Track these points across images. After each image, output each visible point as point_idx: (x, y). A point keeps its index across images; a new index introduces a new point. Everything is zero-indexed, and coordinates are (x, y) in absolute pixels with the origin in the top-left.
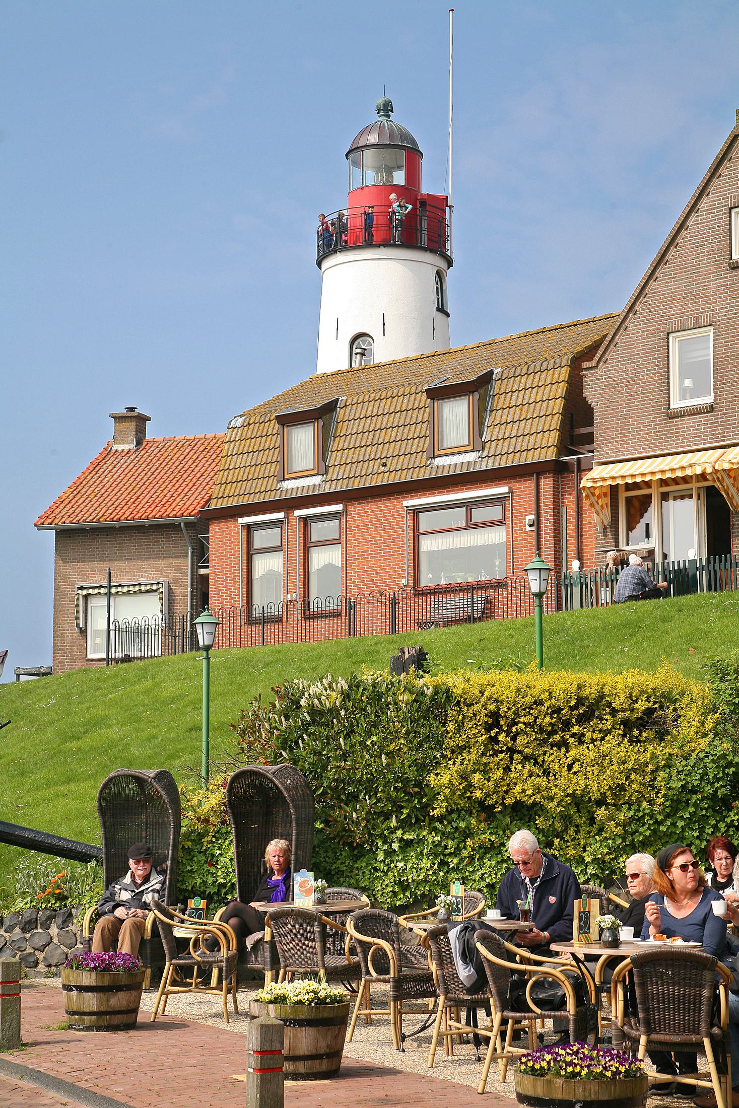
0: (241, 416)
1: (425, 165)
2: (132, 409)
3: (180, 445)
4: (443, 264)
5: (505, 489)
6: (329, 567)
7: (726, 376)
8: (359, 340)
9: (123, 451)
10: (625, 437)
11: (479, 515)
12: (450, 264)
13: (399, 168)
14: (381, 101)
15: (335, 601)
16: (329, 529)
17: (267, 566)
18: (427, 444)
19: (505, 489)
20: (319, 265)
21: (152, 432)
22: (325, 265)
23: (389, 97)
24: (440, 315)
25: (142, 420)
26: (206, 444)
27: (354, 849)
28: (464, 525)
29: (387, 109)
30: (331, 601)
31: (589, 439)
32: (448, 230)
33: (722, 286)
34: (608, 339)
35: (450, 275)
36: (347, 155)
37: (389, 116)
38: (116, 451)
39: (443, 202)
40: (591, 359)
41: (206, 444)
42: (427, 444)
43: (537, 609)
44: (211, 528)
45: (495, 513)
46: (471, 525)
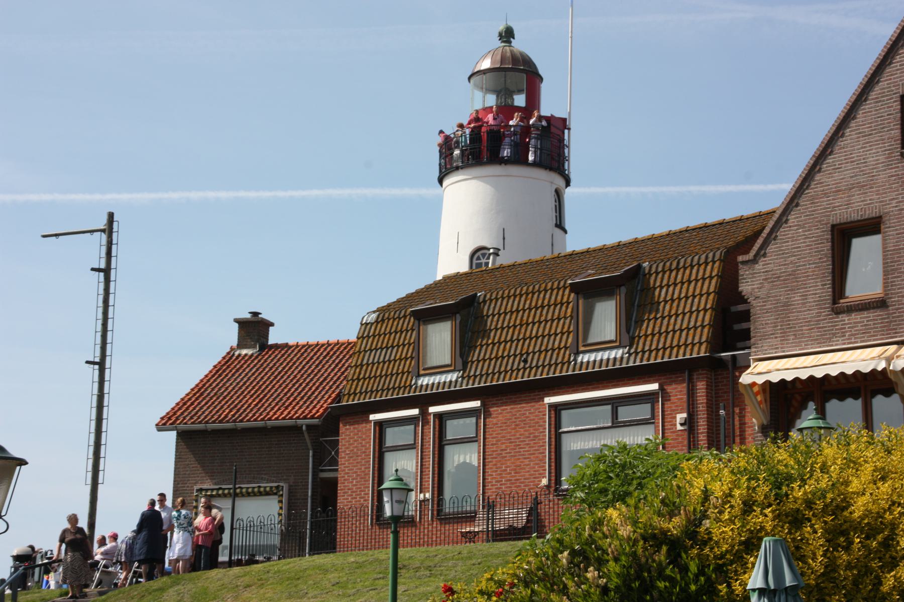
0: (374, 312)
1: (545, 89)
2: (255, 314)
3: (303, 351)
4: (561, 182)
5: (655, 386)
6: (465, 465)
7: (897, 269)
8: (479, 253)
9: (246, 355)
10: (785, 333)
11: (625, 413)
12: (568, 183)
13: (520, 91)
14: (501, 27)
15: (473, 500)
16: (466, 427)
17: (403, 464)
18: (570, 340)
19: (655, 386)
20: (441, 181)
21: (274, 337)
22: (446, 182)
23: (511, 24)
24: (558, 231)
25: (266, 325)
26: (329, 349)
27: (117, 561)
28: (610, 424)
29: (507, 35)
30: (469, 500)
31: (746, 335)
32: (566, 151)
33: (892, 176)
34: (767, 231)
35: (569, 193)
36: (469, 78)
37: (510, 42)
38: (239, 355)
39: (563, 124)
40: (747, 252)
41: (329, 349)
42: (570, 340)
43: (391, 536)
44: (343, 429)
45: (643, 411)
46: (616, 424)
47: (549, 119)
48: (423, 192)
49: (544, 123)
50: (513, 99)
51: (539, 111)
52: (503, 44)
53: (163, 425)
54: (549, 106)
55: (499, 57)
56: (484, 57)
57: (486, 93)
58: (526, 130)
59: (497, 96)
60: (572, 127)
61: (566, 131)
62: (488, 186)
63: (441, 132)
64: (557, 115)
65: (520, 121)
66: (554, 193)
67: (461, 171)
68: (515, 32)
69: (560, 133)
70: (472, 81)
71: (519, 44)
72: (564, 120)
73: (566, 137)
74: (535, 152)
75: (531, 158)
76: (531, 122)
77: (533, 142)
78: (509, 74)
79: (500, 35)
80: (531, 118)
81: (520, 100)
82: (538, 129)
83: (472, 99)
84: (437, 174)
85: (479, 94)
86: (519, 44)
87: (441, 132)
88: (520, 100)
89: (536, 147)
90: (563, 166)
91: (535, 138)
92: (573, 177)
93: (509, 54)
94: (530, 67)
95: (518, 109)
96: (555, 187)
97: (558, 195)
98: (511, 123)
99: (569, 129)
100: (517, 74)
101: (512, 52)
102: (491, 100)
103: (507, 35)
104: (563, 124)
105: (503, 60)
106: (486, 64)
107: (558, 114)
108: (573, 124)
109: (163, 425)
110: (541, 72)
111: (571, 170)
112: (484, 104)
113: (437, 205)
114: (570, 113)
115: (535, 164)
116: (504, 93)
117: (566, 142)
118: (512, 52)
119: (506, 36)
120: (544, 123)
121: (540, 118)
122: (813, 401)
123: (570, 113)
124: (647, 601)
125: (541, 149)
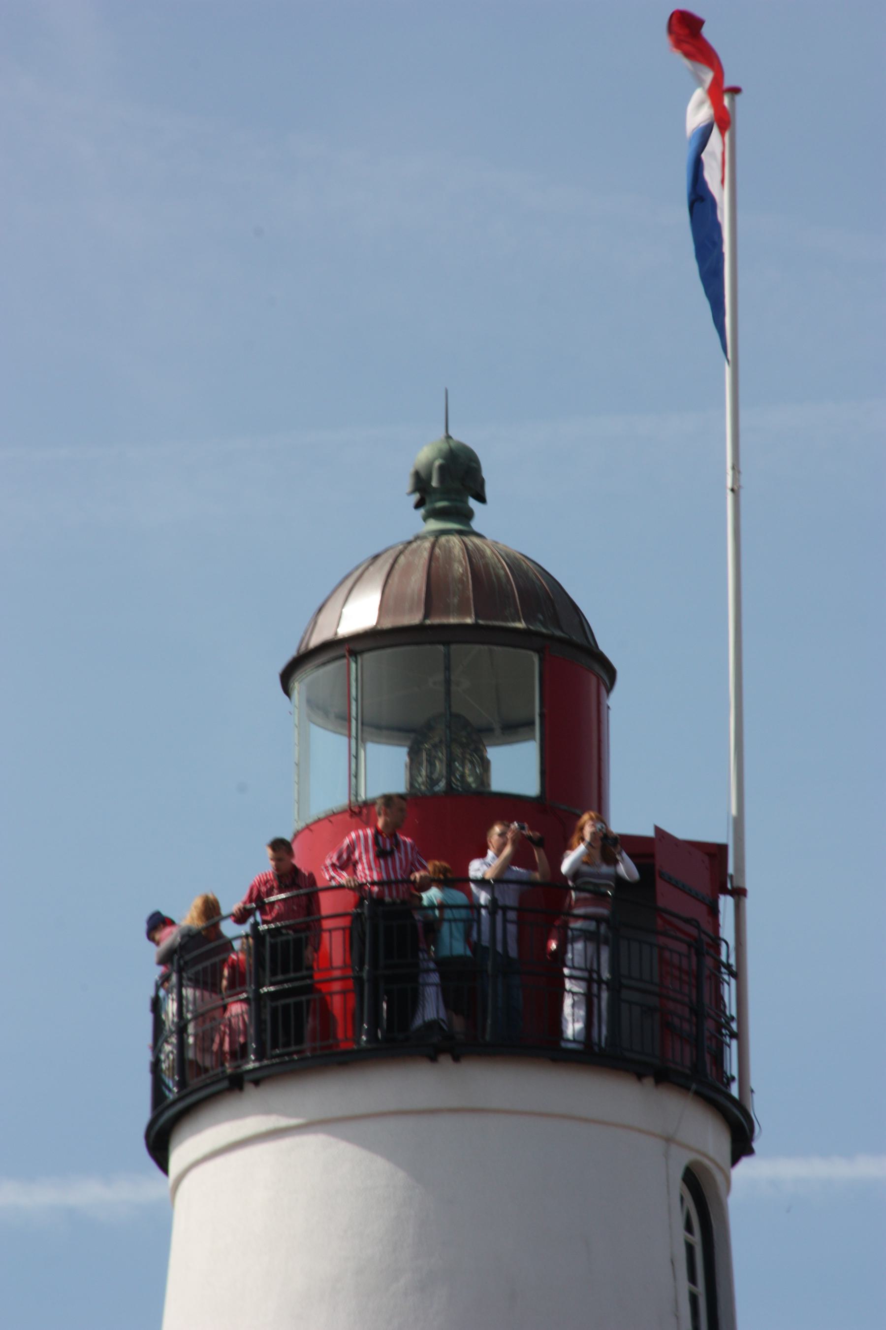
1: (630, 723)
4: (708, 1137)
12: (742, 1143)
13: (512, 730)
14: (425, 452)
20: (159, 1146)
22: (182, 1153)
23: (465, 435)
29: (452, 485)
32: (729, 992)
35: (748, 1185)
36: (286, 677)
37: (467, 516)
39: (711, 869)
47: (650, 850)
48: (89, 1194)
49: (626, 868)
50: (485, 764)
51: (601, 815)
52: (434, 525)
53: (657, 830)
54: (651, 787)
55: (417, 582)
56: (350, 582)
57: (361, 740)
58: (541, 902)
59: (414, 754)
60: (750, 883)
61: (726, 904)
62: (380, 1164)
63: (158, 923)
64: (683, 831)
65: (515, 859)
66: (677, 1185)
67: (252, 1095)
68: (487, 473)
69: (699, 912)
70: (298, 687)
71: (503, 524)
72: (714, 855)
73: (727, 931)
74: (589, 1001)
75: (573, 1025)
76: (565, 867)
77: (577, 951)
78: (468, 654)
79: (420, 483)
80: (566, 846)
81: (515, 768)
82: (598, 896)
83: (302, 767)
84: (142, 1112)
85: (330, 746)
86: (503, 524)
87: (158, 923)
88: (515, 768)
89: (591, 979)
90: (719, 1060)
91: (587, 936)
92: (761, 1109)
93: (460, 568)
94: (556, 621)
95: (510, 806)
96: (680, 1161)
97: (702, 1199)
98: (477, 869)
99: (739, 893)
100: (495, 650)
101: (471, 555)
102: (387, 770)
103: (452, 485)
104: (711, 869)
105: (435, 592)
106: (361, 613)
107: (688, 827)
108: (756, 871)
109: (657, 830)
110: (605, 646)
111: (755, 1081)
112: (353, 789)
113: (147, 1247)
114: (738, 823)
115: (590, 1056)
116: (445, 735)
117: (727, 954)
118: (471, 555)
119: (445, 492)
120: (626, 868)
121: (608, 845)
122: (553, 939)
123: (738, 823)
124: (545, 945)
125: (615, 986)
